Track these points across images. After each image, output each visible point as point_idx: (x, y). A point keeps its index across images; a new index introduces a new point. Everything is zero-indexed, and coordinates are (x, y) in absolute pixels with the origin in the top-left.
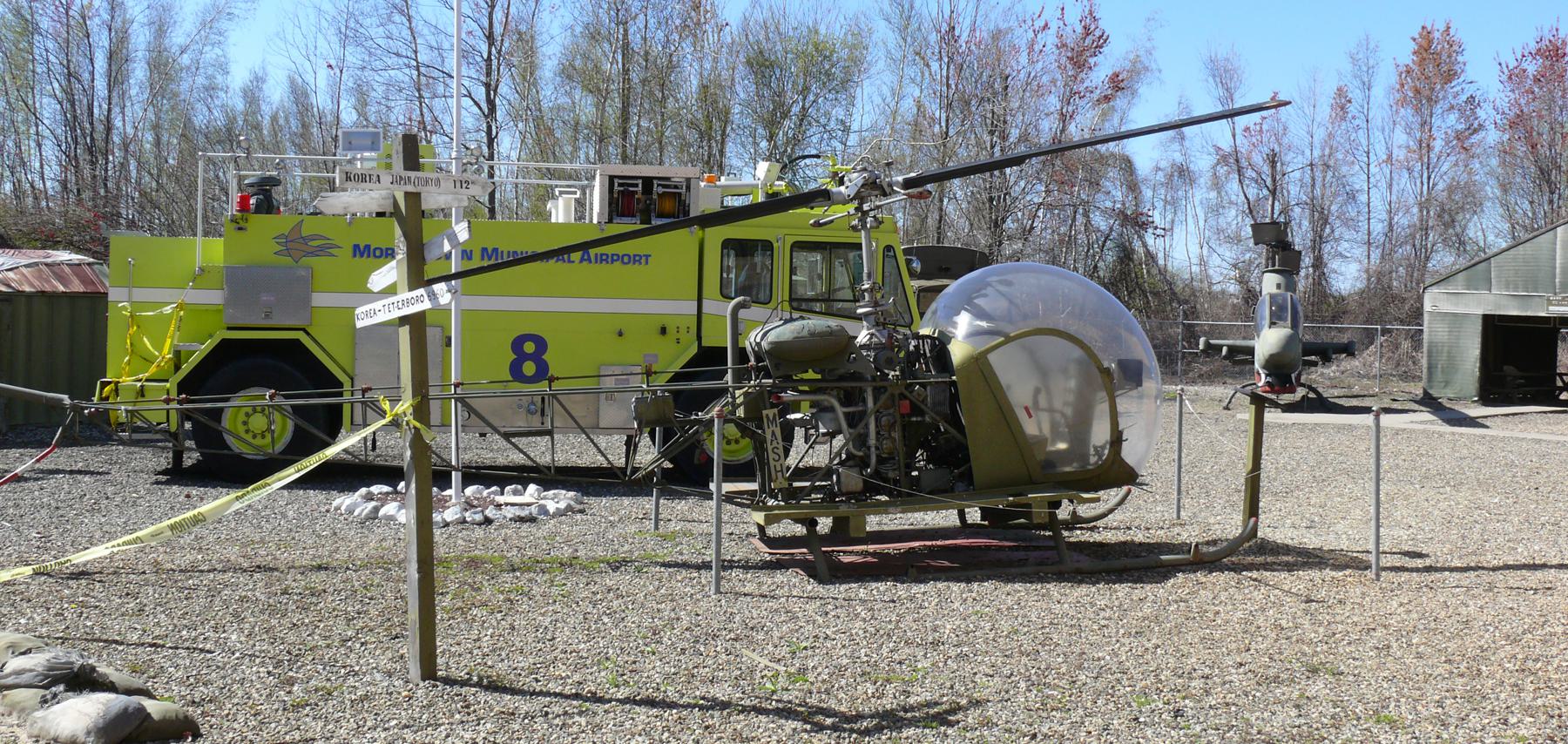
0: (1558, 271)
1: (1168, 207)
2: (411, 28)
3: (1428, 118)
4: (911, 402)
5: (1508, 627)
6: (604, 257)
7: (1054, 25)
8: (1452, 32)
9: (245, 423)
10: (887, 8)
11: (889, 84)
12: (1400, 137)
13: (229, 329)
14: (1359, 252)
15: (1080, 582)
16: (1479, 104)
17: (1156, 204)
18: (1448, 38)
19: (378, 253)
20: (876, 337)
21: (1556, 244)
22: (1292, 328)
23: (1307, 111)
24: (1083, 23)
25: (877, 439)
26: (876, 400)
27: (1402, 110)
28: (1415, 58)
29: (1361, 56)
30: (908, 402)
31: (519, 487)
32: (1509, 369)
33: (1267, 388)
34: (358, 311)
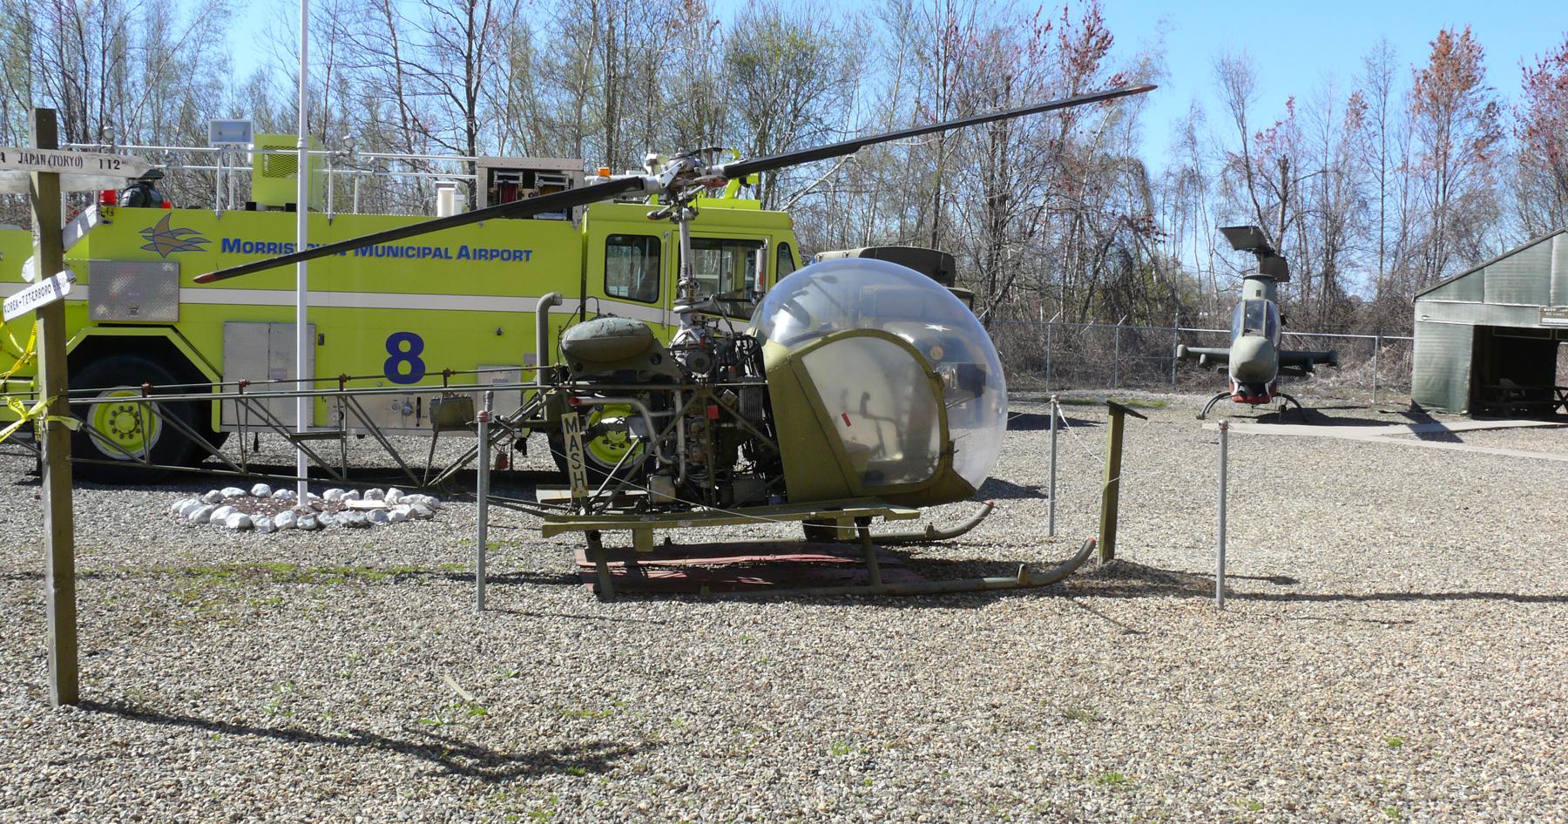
0: (1552, 281)
1: (1179, 213)
2: (390, 25)
3: (1446, 125)
4: (720, 407)
5: (1332, 667)
6: (483, 253)
7: (1056, 25)
8: (1472, 37)
9: (112, 422)
10: (884, 6)
11: (886, 83)
12: (1416, 145)
13: (101, 325)
14: (1371, 261)
15: (890, 605)
16: (1498, 111)
17: (1166, 210)
18: (1467, 43)
19: (248, 248)
20: (692, 336)
21: (1551, 253)
22: (1266, 337)
23: (1322, 117)
24: (1087, 24)
25: (687, 446)
26: (684, 404)
27: (1418, 116)
28: (1433, 64)
29: (1377, 61)
30: (716, 406)
31: (380, 491)
32: (1506, 382)
33: (1240, 398)
34: (7, 302)
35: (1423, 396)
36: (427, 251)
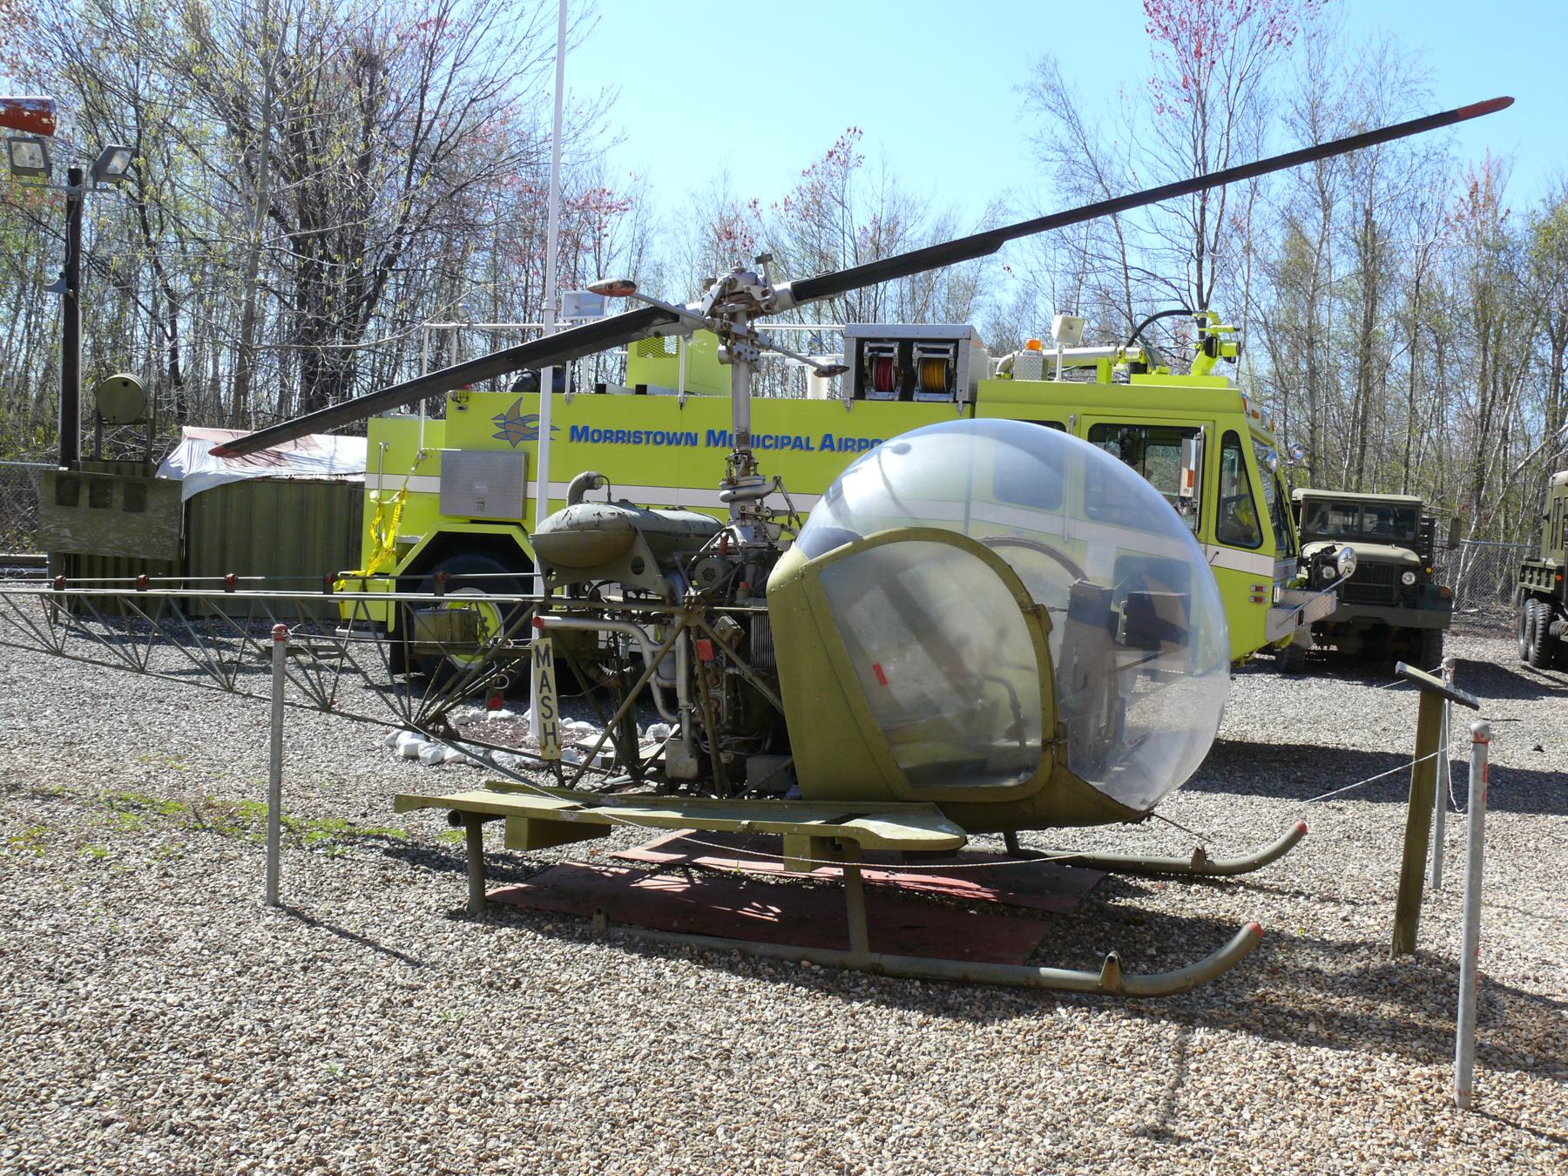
13: (473, 522)
19: (596, 437)
35: (931, 697)
36: (863, 444)
